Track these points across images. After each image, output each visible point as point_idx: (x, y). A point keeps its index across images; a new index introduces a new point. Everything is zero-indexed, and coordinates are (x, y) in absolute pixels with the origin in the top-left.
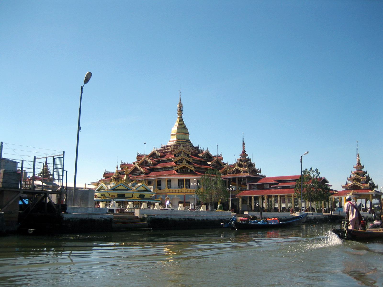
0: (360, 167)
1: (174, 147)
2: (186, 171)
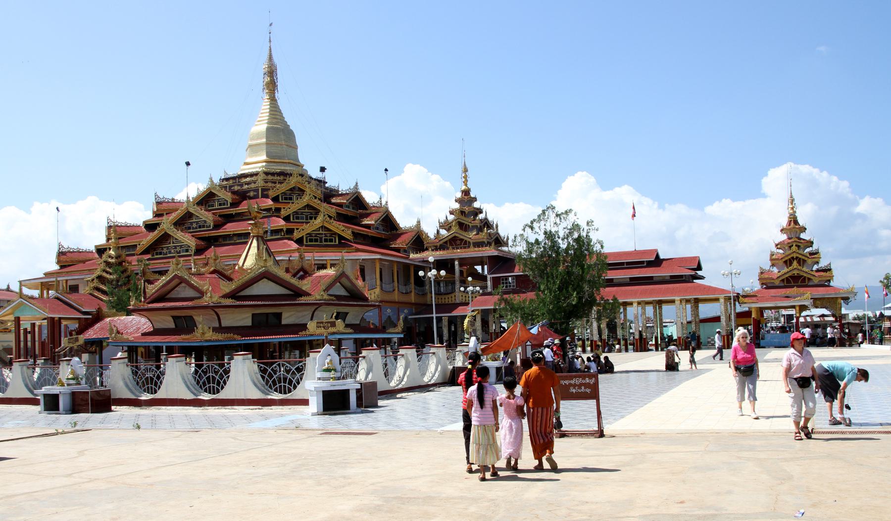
0: (467, 198)
1: (266, 177)
2: (326, 240)
